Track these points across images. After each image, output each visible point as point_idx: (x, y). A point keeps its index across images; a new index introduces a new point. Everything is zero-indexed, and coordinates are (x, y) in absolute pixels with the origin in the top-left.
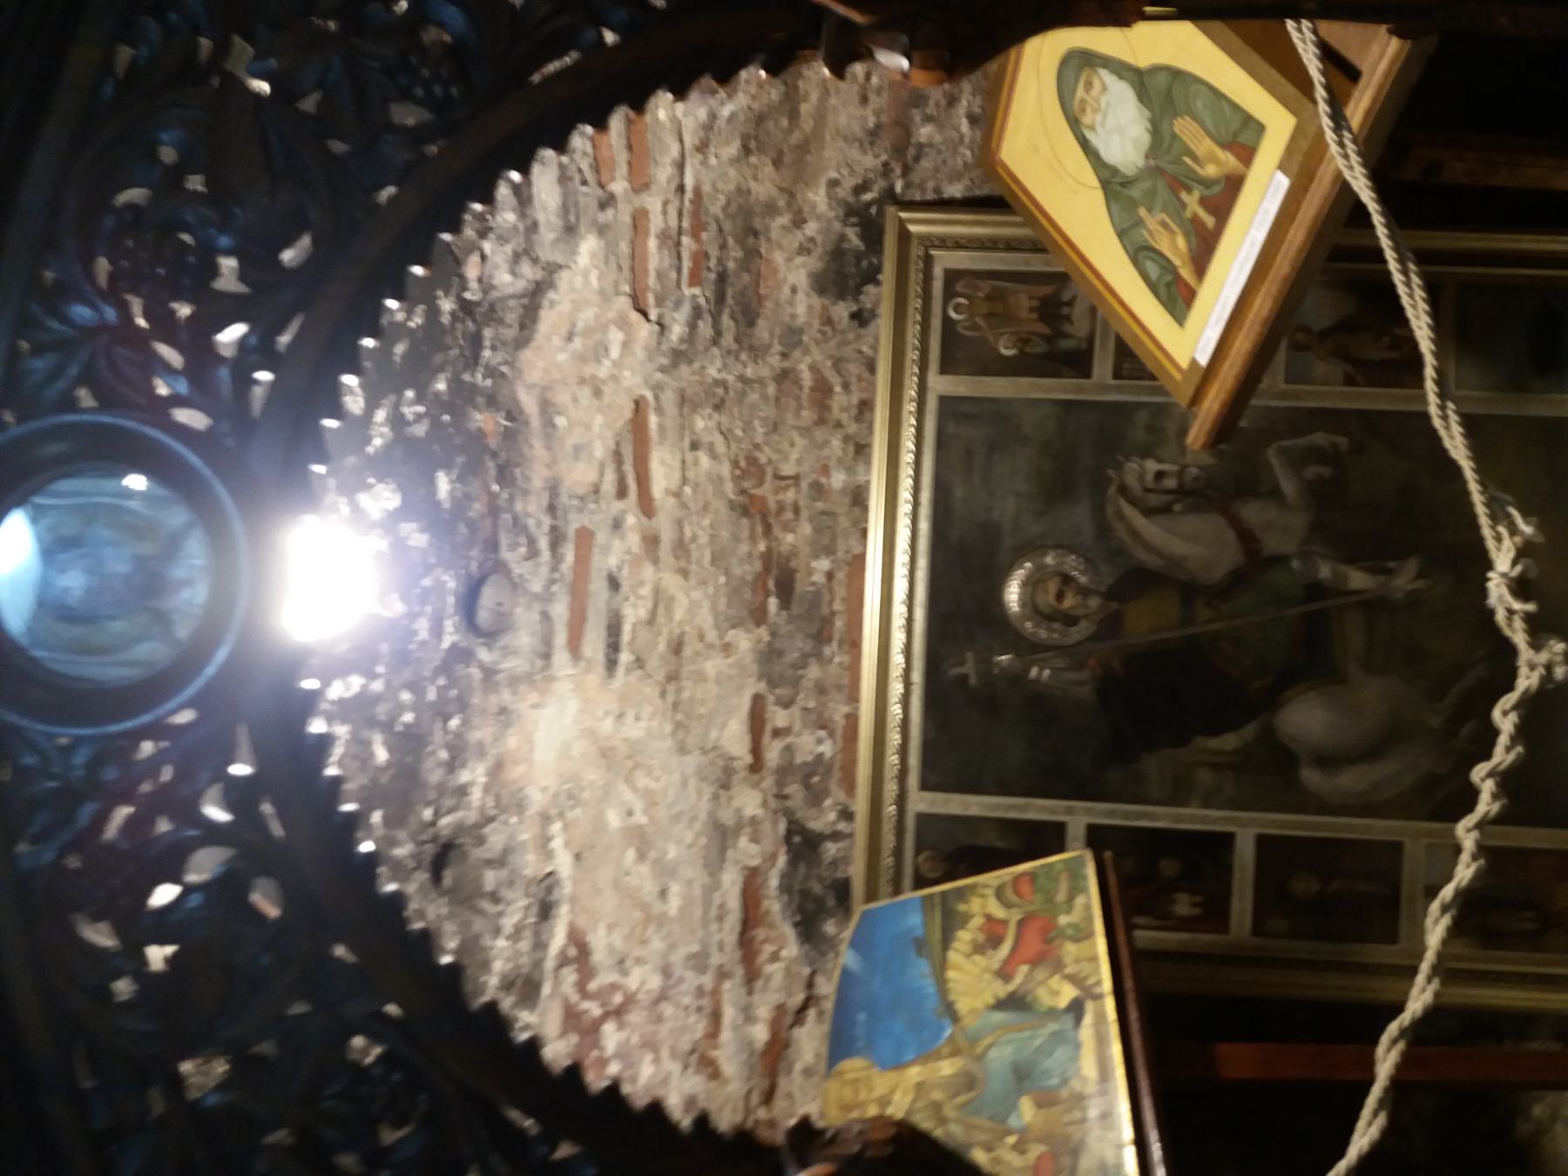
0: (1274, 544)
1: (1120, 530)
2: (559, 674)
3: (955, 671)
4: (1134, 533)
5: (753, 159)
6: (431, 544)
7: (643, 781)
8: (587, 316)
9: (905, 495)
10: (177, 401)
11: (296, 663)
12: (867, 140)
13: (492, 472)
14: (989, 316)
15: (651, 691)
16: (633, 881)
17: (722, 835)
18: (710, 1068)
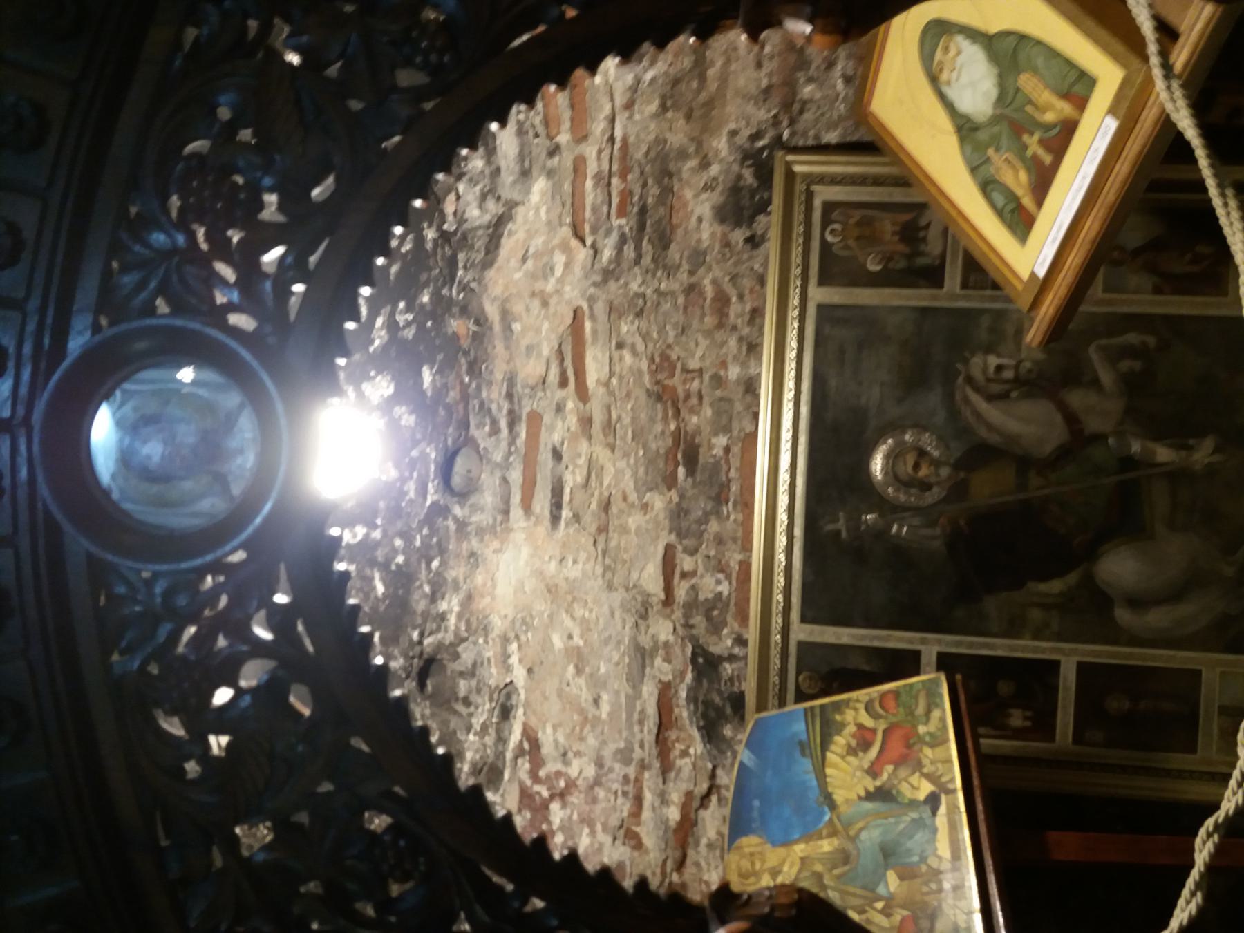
0: (1093, 425)
1: (967, 413)
2: (515, 526)
3: (830, 527)
4: (978, 415)
5: (669, 115)
6: (416, 424)
7: (579, 612)
8: (538, 242)
9: (789, 383)
10: (231, 307)
11: (322, 516)
12: (762, 97)
13: (464, 368)
14: (858, 238)
15: (586, 540)
16: (574, 690)
17: (642, 656)
18: (635, 842)
